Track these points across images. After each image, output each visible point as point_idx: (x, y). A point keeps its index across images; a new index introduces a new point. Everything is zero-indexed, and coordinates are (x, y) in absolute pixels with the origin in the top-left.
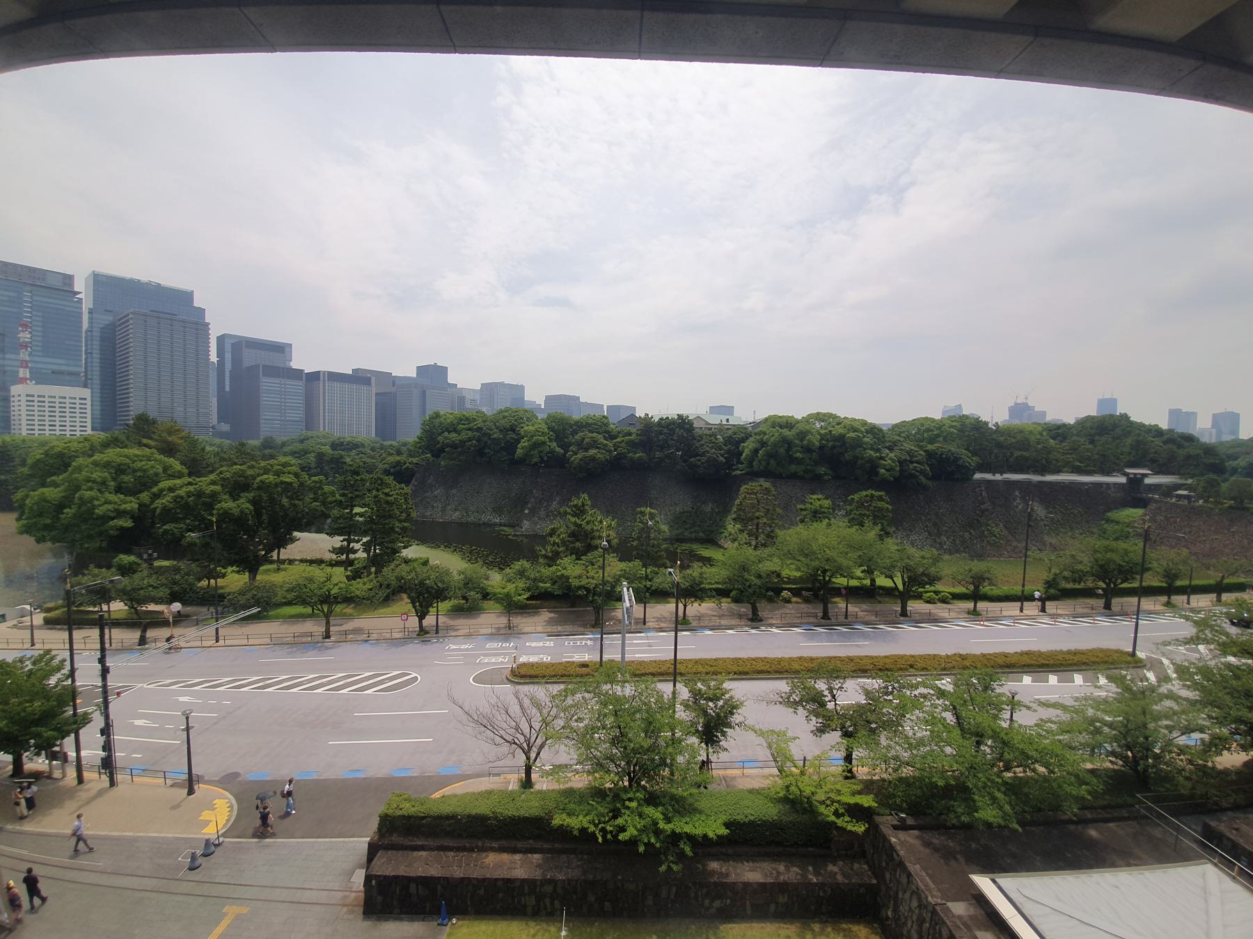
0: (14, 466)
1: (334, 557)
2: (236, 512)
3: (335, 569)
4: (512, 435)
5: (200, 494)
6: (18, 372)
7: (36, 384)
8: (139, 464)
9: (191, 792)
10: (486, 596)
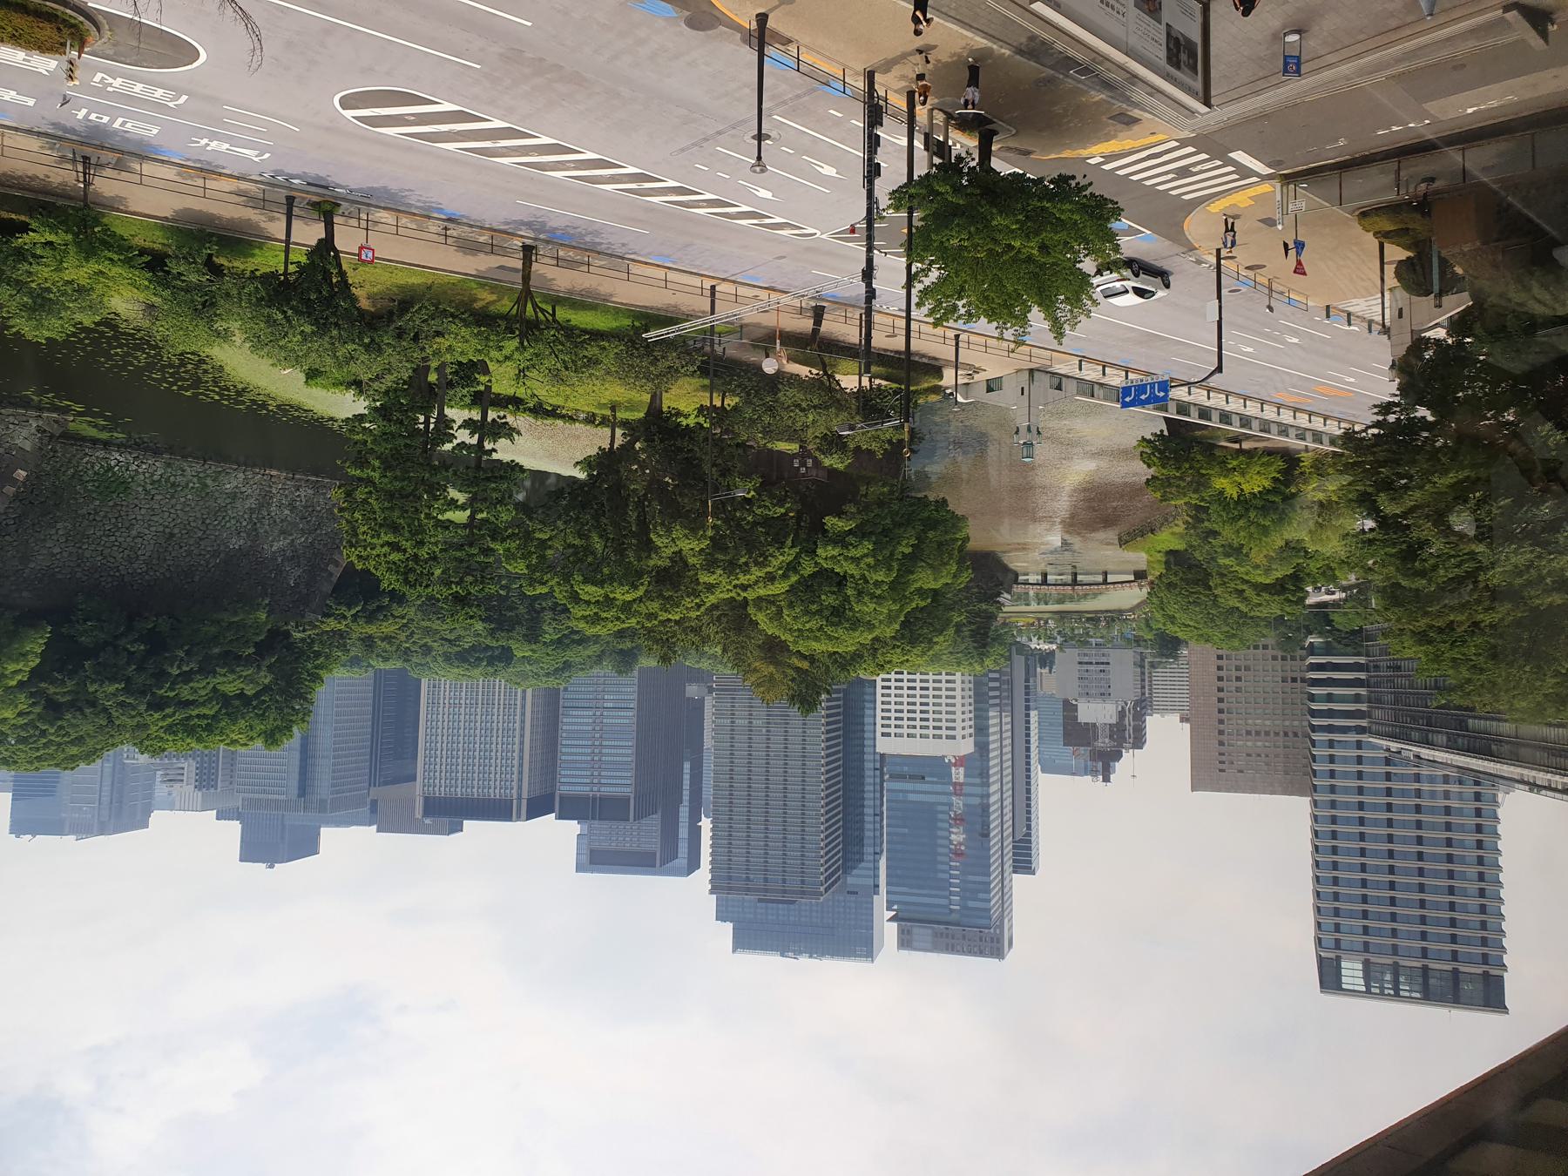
0: (970, 623)
1: (510, 419)
2: (678, 532)
3: (510, 392)
4: (59, 691)
5: (732, 568)
6: (966, 776)
7: (944, 757)
8: (813, 624)
9: (762, 19)
10: (155, 263)
